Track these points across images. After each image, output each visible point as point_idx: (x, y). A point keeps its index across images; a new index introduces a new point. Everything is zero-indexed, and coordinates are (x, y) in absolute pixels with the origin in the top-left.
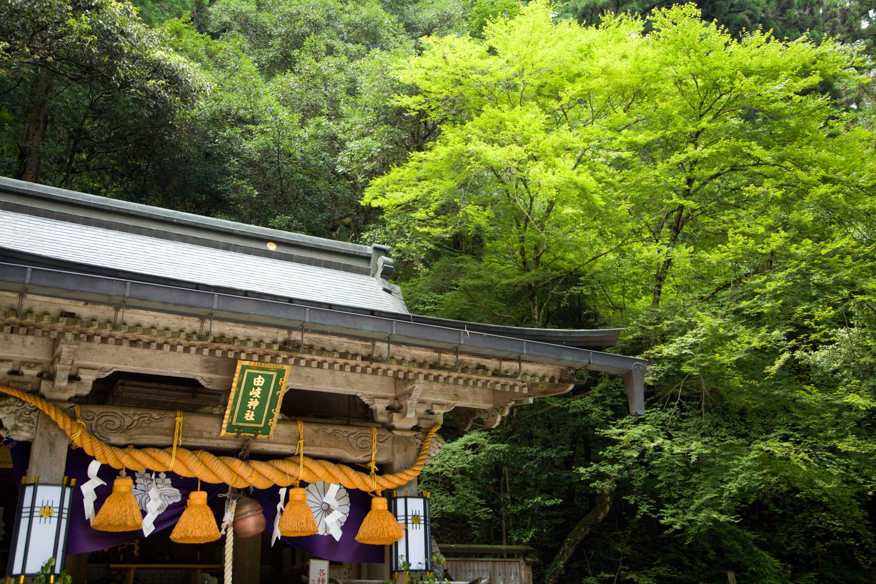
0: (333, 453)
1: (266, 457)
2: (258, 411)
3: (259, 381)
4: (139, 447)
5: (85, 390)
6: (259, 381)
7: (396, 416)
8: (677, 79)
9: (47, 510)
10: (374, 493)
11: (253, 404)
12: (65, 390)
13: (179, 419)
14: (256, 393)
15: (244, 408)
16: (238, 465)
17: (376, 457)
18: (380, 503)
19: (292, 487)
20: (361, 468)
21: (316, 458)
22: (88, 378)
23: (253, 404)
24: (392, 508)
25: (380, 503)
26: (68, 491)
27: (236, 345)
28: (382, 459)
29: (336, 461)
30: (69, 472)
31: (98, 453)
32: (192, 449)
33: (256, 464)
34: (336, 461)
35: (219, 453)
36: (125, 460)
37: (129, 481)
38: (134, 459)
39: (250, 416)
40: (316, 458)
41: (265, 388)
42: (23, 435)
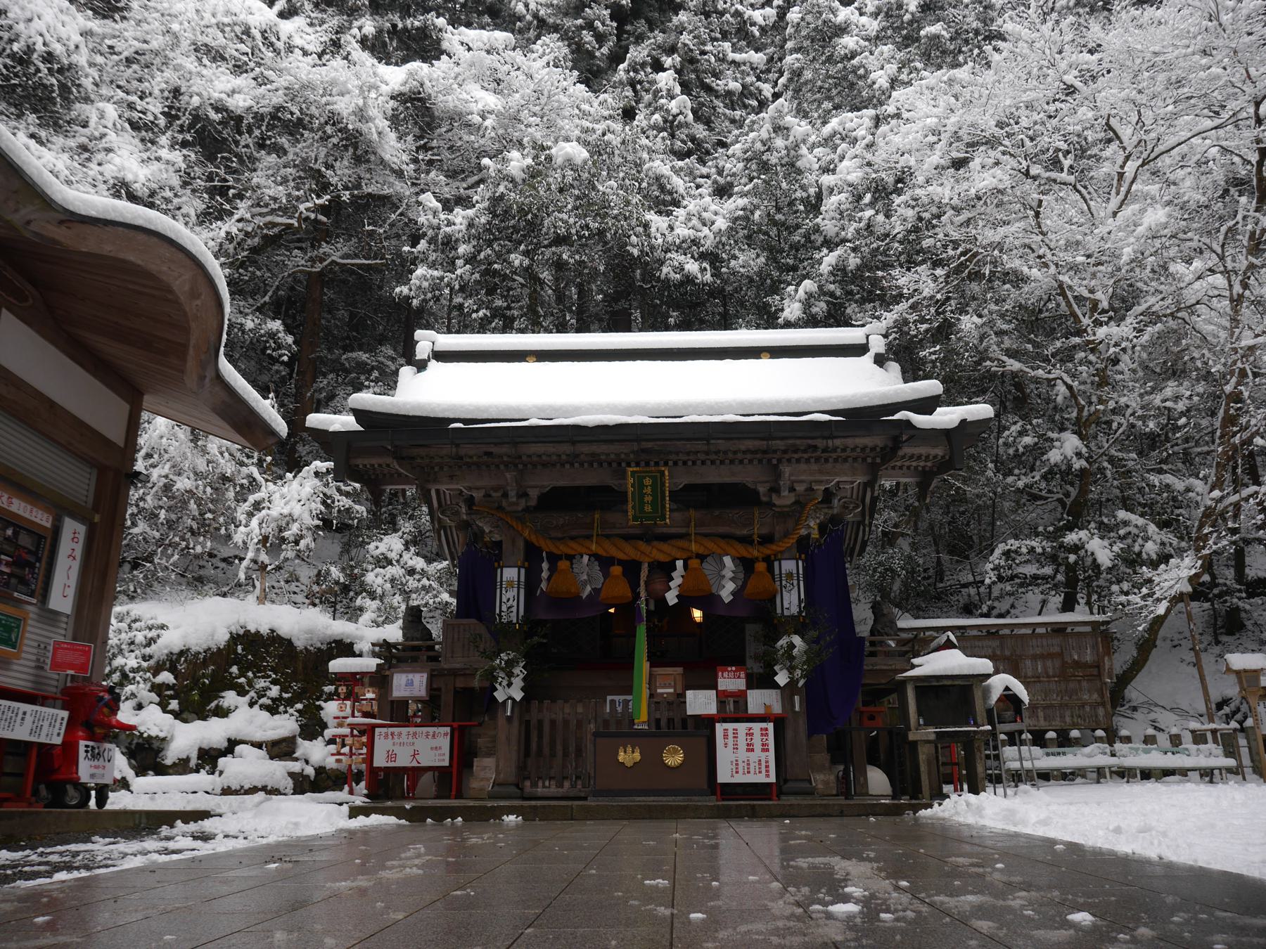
0: (722, 530)
1: (665, 538)
2: (653, 503)
3: (648, 481)
4: (572, 538)
5: (533, 503)
6: (648, 481)
7: (774, 496)
8: (238, 29)
9: (510, 583)
10: (757, 558)
11: (648, 499)
12: (517, 504)
13: (597, 516)
14: (649, 490)
15: (642, 503)
16: (642, 545)
17: (757, 530)
18: (761, 566)
19: (690, 558)
20: (746, 540)
21: (706, 535)
22: (534, 494)
23: (648, 499)
24: (770, 569)
25: (761, 566)
26: (523, 571)
27: (779, 455)
28: (764, 531)
29: (724, 537)
30: (527, 558)
31: (675, 553)
32: (608, 537)
33: (655, 543)
34: (724, 537)
35: (627, 538)
36: (563, 549)
37: (568, 563)
38: (659, 550)
39: (648, 508)
40: (706, 535)
41: (654, 486)
42: (497, 537)
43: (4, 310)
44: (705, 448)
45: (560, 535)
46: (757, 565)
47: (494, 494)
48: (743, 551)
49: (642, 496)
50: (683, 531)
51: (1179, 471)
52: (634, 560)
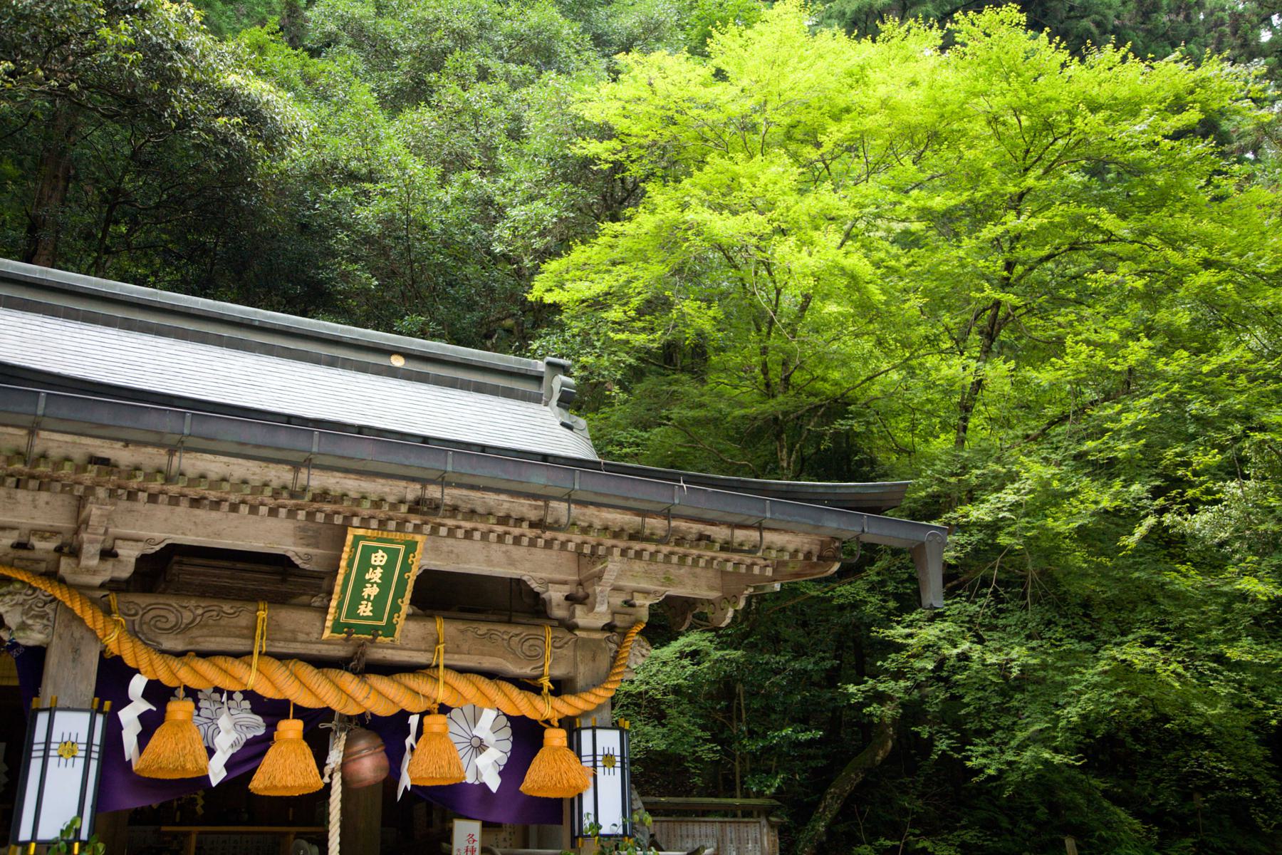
0: (488, 663)
1: (389, 669)
2: (378, 602)
3: (379, 558)
5: (125, 572)
6: (379, 558)
7: (579, 610)
9: (69, 747)
10: (547, 722)
11: (371, 591)
13: (262, 614)
14: (376, 575)
15: (357, 598)
16: (349, 681)
17: (550, 669)
20: (528, 685)
21: (462, 671)
22: (129, 554)
23: (371, 591)
24: (574, 744)
25: (556, 738)
28: (559, 672)
29: (491, 675)
32: (282, 657)
35: (320, 663)
36: (184, 674)
39: (365, 609)
40: (462, 671)
41: (388, 569)
42: (34, 638)
43: (214, 784)
44: (533, 515)
45: (180, 647)
46: (549, 733)
47: (39, 545)
48: (526, 705)
49: (361, 583)
50: (421, 658)
51: (848, 572)
52: (328, 708)
